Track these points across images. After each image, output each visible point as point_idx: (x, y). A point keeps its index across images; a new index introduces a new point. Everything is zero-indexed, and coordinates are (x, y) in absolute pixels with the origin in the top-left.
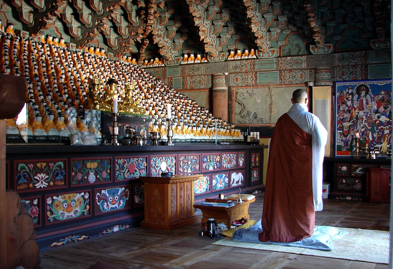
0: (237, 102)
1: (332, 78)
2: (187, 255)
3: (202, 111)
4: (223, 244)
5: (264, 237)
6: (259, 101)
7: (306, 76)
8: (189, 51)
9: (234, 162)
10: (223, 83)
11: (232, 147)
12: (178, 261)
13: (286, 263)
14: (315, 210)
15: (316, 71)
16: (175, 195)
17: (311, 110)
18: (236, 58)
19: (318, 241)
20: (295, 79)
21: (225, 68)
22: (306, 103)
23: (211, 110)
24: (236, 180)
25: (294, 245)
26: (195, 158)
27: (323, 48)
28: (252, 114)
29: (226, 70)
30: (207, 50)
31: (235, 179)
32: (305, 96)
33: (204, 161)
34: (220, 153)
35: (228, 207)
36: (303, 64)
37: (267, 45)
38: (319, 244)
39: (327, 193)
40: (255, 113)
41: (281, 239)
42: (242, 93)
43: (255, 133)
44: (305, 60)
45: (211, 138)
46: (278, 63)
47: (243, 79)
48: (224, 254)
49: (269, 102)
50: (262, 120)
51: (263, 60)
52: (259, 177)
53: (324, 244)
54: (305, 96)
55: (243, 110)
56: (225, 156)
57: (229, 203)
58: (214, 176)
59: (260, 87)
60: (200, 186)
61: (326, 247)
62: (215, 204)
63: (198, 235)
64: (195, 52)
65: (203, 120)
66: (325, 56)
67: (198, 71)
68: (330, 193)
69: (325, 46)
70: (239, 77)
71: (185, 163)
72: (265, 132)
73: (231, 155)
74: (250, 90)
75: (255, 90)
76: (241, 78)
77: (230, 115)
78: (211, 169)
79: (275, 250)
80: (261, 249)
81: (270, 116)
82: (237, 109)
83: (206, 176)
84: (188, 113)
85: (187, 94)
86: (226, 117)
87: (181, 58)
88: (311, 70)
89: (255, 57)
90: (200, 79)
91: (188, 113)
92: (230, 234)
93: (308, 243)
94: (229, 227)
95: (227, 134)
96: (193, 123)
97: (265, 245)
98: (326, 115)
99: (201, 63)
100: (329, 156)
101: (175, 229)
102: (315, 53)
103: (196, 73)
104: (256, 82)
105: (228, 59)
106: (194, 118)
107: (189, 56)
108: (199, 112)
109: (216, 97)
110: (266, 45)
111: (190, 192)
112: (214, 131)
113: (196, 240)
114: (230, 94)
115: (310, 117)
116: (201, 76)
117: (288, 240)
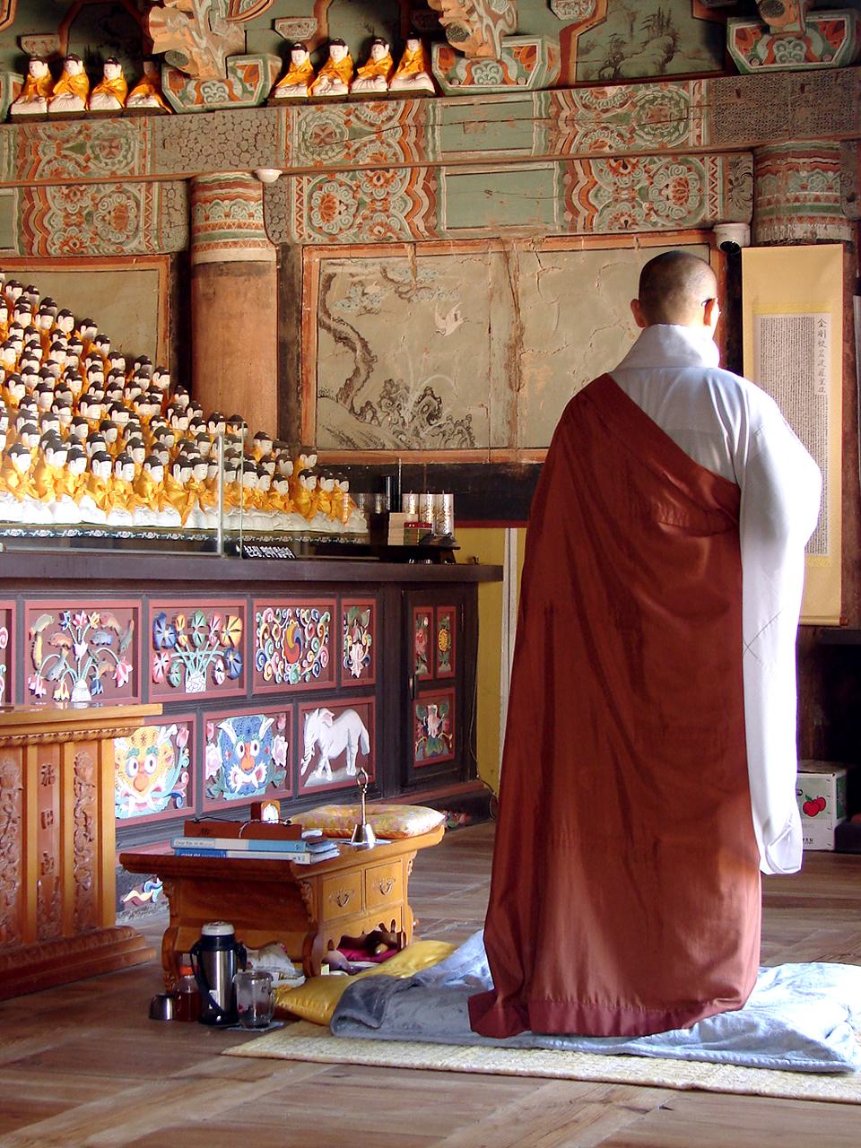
0: (329, 329)
1: (851, 199)
2: (105, 1102)
3: (137, 380)
4: (283, 1052)
5: (501, 1010)
6: (450, 327)
7: (707, 190)
8: (54, 44)
9: (319, 653)
10: (249, 226)
11: (311, 570)
12: (62, 1126)
13: (620, 1124)
14: (764, 867)
15: (761, 160)
16: (16, 813)
17: (733, 359)
18: (322, 87)
19: (780, 1025)
20: (645, 205)
21: (256, 147)
22: (706, 321)
23: (186, 373)
24: (330, 752)
25: (655, 1049)
26: (112, 623)
27: (801, 37)
28: (414, 397)
29: (267, 152)
30: (161, 40)
31: (323, 744)
32: (703, 285)
33: (160, 643)
34: (243, 602)
35: (305, 859)
36: (692, 124)
37: (496, 18)
38: (786, 1040)
39: (829, 819)
40: (428, 392)
41: (590, 1022)
42: (355, 285)
43: (430, 497)
44: (699, 105)
45: (190, 524)
46: (551, 121)
47: (360, 204)
48: (296, 1095)
49: (502, 333)
50: (464, 428)
51: (474, 100)
52: (457, 737)
53: (810, 1042)
54: (703, 285)
55: (363, 372)
56: (271, 618)
57: (313, 842)
58: (211, 726)
59: (453, 250)
60: (141, 779)
61: (826, 1054)
62: (236, 848)
63: (146, 1016)
64: (93, 49)
65: (145, 427)
66: (813, 81)
67: (111, 155)
68: (849, 819)
69: (808, 25)
70: (341, 195)
71: (59, 648)
72: (486, 492)
73: (304, 614)
74: (399, 264)
75: (428, 267)
76: (351, 201)
77: (292, 404)
78: (196, 684)
79: (558, 1072)
80: (487, 1068)
81: (513, 407)
82: (328, 366)
83: (168, 725)
84: (61, 387)
85: (47, 282)
86: (266, 413)
87: (15, 79)
88: (732, 158)
89: (425, 84)
90: (123, 199)
91: (61, 387)
92: (319, 1006)
93: (727, 1037)
94: (310, 973)
95: (279, 503)
96: (92, 438)
97: (504, 1053)
98: (814, 399)
99: (125, 113)
100: (837, 622)
101: (18, 995)
102: (755, 67)
103: (99, 169)
104: (433, 220)
105: (280, 94)
106: (94, 412)
107: (57, 69)
108: (121, 381)
109: (210, 300)
110: (488, 20)
111: (95, 799)
112: (209, 484)
113: (136, 1039)
114: (292, 285)
115: (797, 890)
116: (126, 186)
117: (627, 1022)
